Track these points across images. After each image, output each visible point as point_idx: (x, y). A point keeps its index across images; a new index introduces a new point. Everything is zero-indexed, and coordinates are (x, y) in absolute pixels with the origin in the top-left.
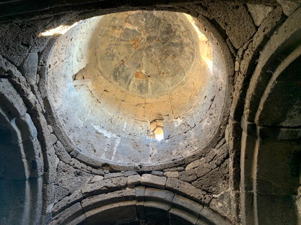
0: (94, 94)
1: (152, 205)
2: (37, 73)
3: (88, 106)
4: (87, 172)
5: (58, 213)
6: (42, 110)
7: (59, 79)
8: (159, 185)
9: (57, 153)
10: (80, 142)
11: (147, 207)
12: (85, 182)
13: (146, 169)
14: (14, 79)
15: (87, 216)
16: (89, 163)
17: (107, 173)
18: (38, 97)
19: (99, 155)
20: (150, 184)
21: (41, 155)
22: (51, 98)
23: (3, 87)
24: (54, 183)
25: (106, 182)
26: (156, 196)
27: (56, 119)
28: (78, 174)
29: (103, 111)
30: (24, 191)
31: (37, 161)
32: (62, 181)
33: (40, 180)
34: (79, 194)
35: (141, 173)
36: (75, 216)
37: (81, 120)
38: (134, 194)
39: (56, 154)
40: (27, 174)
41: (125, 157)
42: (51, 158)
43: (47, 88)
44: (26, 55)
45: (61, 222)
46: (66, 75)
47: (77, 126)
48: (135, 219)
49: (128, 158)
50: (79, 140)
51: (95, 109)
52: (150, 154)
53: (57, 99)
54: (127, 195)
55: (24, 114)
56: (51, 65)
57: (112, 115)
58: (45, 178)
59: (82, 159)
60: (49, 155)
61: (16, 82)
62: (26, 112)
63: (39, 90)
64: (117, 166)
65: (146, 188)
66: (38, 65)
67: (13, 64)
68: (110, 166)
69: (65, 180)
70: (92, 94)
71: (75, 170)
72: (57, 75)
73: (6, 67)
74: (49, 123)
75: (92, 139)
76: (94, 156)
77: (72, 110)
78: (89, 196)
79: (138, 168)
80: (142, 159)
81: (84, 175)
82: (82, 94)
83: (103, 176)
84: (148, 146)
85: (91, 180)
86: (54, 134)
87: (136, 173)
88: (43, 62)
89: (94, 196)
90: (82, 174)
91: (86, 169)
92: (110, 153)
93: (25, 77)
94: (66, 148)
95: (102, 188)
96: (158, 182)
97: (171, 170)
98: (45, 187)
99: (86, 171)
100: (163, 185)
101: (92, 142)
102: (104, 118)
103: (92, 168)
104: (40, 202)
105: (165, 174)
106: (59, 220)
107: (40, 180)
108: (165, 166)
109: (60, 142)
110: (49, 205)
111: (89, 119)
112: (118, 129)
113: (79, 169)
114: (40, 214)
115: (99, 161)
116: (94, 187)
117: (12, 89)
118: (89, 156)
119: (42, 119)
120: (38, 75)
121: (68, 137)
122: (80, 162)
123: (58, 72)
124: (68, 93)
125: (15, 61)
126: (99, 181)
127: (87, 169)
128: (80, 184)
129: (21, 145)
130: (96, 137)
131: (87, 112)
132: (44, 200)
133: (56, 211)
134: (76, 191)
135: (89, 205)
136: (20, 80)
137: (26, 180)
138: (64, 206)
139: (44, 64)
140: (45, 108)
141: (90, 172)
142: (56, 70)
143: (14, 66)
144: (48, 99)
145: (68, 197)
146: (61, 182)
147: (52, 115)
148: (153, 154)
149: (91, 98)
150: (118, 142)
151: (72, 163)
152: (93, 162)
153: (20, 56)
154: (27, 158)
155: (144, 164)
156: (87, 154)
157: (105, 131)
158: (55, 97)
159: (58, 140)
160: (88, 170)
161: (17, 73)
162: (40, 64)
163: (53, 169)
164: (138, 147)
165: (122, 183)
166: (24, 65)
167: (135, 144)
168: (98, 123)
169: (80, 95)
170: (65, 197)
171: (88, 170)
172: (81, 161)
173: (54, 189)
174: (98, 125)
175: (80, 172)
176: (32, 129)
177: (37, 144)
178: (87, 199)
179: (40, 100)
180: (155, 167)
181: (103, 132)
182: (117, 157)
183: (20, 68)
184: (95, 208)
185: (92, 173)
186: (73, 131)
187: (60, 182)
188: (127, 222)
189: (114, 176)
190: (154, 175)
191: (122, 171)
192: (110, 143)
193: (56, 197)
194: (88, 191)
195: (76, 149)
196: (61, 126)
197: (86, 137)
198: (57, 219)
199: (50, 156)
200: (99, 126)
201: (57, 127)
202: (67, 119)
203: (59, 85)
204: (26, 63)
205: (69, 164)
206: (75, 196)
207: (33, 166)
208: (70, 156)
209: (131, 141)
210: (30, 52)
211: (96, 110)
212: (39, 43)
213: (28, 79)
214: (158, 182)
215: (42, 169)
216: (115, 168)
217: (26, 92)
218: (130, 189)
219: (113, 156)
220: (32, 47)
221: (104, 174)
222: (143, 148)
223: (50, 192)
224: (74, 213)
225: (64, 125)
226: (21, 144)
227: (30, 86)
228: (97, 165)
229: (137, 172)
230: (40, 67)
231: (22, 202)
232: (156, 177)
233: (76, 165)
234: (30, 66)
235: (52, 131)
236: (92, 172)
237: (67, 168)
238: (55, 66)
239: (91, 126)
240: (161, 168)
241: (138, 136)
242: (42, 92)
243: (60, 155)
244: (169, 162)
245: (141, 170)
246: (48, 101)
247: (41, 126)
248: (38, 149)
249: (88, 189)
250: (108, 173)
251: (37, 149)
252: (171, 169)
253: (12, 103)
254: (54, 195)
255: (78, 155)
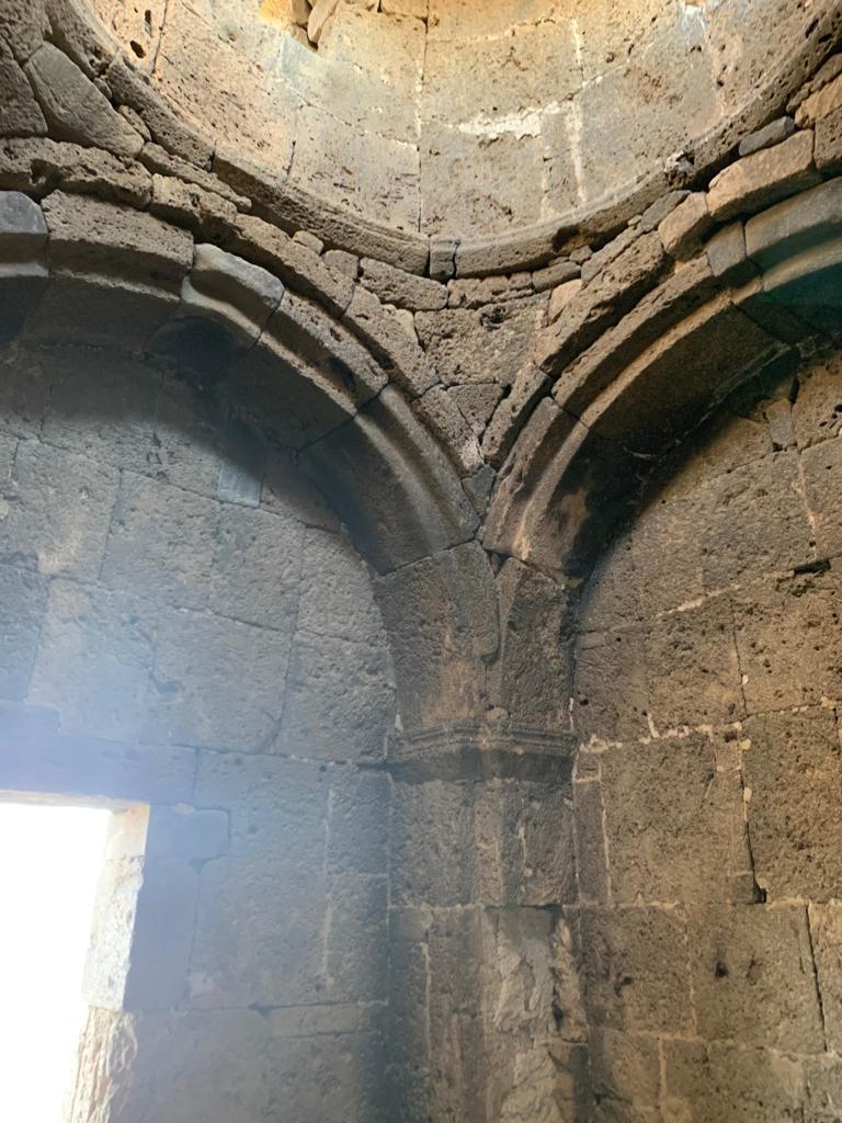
0: (397, 9)
1: (796, 272)
2: (116, 106)
3: (397, 72)
4: (520, 297)
5: (503, 454)
6: (237, 204)
7: (216, 64)
8: (784, 179)
9: (387, 299)
10: (441, 217)
11: (782, 288)
12: (533, 330)
13: (716, 154)
14: (72, 179)
15: (590, 424)
16: (506, 264)
17: (585, 260)
18: (188, 176)
19: (531, 217)
20: (750, 197)
21: (340, 330)
22: (231, 150)
23: (64, 223)
24: (440, 382)
25: (596, 291)
26: (792, 232)
27: (301, 199)
28: (497, 318)
29: (465, 45)
30: (372, 445)
31: (337, 354)
32: (459, 367)
33: (390, 398)
34: (532, 376)
35: (701, 183)
36: (557, 438)
37: (404, 141)
38: (706, 273)
39: (383, 302)
40: (345, 402)
41: (627, 162)
42: (374, 322)
43: (187, 127)
44: (24, 82)
45: (525, 473)
46: (231, 30)
47: (400, 169)
48: (774, 352)
49: (637, 156)
50: (434, 212)
51: (430, 66)
52: (715, 81)
53: (262, 133)
54: (681, 291)
55: (190, 251)
56: (138, 41)
57: (508, 33)
58: (398, 382)
59: (478, 267)
60: (362, 320)
61: (84, 181)
62: (195, 243)
63: (171, 151)
64: (602, 215)
65: (744, 225)
66: (92, 80)
67: (28, 137)
68: (581, 231)
69: (467, 358)
70: (388, 14)
71: (477, 314)
72: (193, 57)
73: (15, 162)
74: (291, 231)
75: (479, 177)
76: (508, 232)
77: (347, 133)
78: (567, 365)
79: (680, 169)
80: (691, 122)
81: (514, 313)
82: (349, 44)
83: (578, 275)
84: (700, 49)
85: (546, 314)
86: (335, 247)
87: (681, 193)
88: (93, 57)
89: (582, 355)
90: (507, 311)
91: (512, 289)
92: (566, 184)
93: (98, 147)
94: (403, 265)
95: (589, 316)
96: (779, 172)
97: (819, 82)
98: (419, 409)
99: (515, 293)
100: (800, 172)
101: (485, 188)
102: (483, 72)
103: (528, 275)
104: (432, 452)
105: (798, 117)
106: (516, 470)
107: (390, 398)
108: (786, 83)
109: (371, 261)
110: (460, 447)
111: (429, 117)
112: (553, 75)
113: (488, 302)
114: (453, 479)
115: (535, 235)
116: (564, 330)
117: (94, 209)
118: (496, 242)
119: (258, 230)
120: (125, 109)
121: (383, 229)
122: (478, 281)
123: (189, 40)
124: (287, 86)
125: (22, 123)
126: (573, 301)
127: (514, 286)
128: (521, 344)
129: (266, 339)
130: (489, 164)
131: (410, 98)
132: (442, 441)
133: (495, 452)
134: (520, 372)
135: (577, 389)
136: (90, 167)
137: (352, 418)
138: (506, 429)
139: (103, 60)
140: (241, 189)
141: (530, 291)
142: (172, 43)
143: (37, 141)
144: (222, 158)
145: (506, 400)
146: (458, 370)
147: (278, 198)
148: (730, 69)
149: (396, 31)
150: (575, 123)
151: (455, 300)
152: (517, 253)
153: (16, 98)
154: (311, 362)
155: (699, 139)
156: (482, 241)
157: (511, 115)
158: (249, 133)
159: (361, 256)
160: (518, 290)
161: (60, 154)
162: (93, 70)
163: (407, 350)
164: (663, 86)
165: (646, 262)
166: (55, 111)
167: (645, 80)
168: (469, 105)
169: (342, 58)
170: (499, 403)
171: (518, 290)
172: (481, 276)
173: (450, 399)
174: (473, 114)
175: (497, 310)
176: (250, 278)
177: (300, 309)
178: (564, 376)
179: (201, 181)
180: (743, 119)
181: (507, 127)
182: (598, 181)
183: (59, 132)
184: (603, 388)
185: (538, 291)
186: (395, 195)
187: (456, 373)
188: (754, 374)
189: (613, 254)
190: (753, 152)
191: (630, 222)
192: (548, 148)
193: (471, 419)
194: (553, 353)
195: (435, 249)
196: (336, 212)
197: (452, 188)
198: (509, 470)
199: (367, 318)
200: (481, 115)
201: (324, 221)
202: (349, 172)
203: (234, 84)
204: (54, 102)
205: (447, 306)
206: (522, 388)
207: (341, 373)
208: (434, 282)
209: (626, 82)
210: (22, 63)
211: (438, 62)
212: (11, 10)
213: (110, 147)
214: (775, 172)
215: (372, 368)
216: (601, 226)
217: (137, 189)
218: (688, 265)
219: (580, 189)
220: (10, 41)
221: (578, 267)
222: (680, 75)
223: (441, 412)
224: (545, 432)
225: (350, 197)
226: (263, 336)
227: (136, 159)
228: (538, 254)
229: (683, 188)
230: (103, 77)
231: (388, 473)
232: (761, 156)
233: (472, 298)
234: (72, 101)
235: (321, 243)
236: (536, 285)
237: (450, 322)
238: (156, 33)
239: (449, 136)
240: (775, 104)
241: (643, 39)
242: (187, 153)
243: (403, 298)
244: (793, 54)
245: (693, 170)
246: (227, 164)
247: (270, 253)
248: (320, 326)
249: (551, 344)
250: (586, 256)
251: (317, 323)
252: (816, 77)
253: (128, 245)
254: (463, 416)
255: (456, 261)
